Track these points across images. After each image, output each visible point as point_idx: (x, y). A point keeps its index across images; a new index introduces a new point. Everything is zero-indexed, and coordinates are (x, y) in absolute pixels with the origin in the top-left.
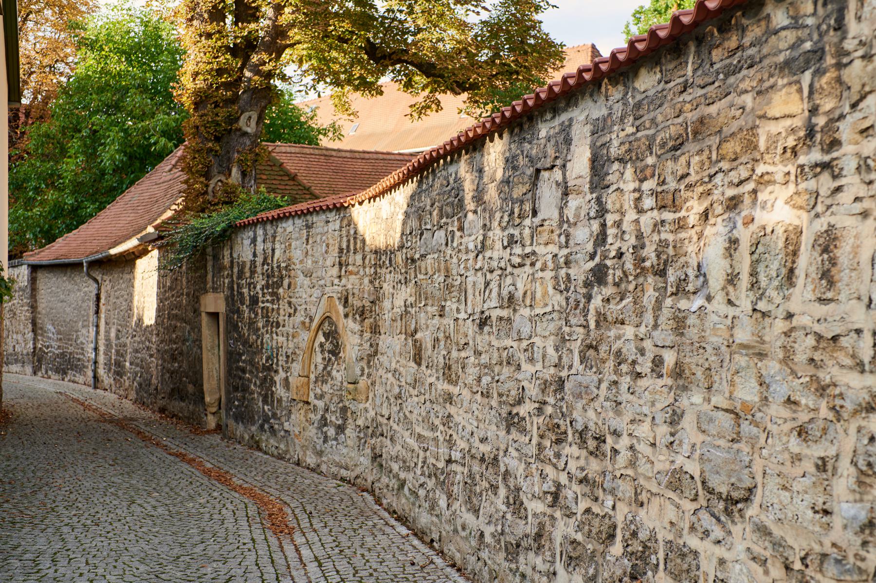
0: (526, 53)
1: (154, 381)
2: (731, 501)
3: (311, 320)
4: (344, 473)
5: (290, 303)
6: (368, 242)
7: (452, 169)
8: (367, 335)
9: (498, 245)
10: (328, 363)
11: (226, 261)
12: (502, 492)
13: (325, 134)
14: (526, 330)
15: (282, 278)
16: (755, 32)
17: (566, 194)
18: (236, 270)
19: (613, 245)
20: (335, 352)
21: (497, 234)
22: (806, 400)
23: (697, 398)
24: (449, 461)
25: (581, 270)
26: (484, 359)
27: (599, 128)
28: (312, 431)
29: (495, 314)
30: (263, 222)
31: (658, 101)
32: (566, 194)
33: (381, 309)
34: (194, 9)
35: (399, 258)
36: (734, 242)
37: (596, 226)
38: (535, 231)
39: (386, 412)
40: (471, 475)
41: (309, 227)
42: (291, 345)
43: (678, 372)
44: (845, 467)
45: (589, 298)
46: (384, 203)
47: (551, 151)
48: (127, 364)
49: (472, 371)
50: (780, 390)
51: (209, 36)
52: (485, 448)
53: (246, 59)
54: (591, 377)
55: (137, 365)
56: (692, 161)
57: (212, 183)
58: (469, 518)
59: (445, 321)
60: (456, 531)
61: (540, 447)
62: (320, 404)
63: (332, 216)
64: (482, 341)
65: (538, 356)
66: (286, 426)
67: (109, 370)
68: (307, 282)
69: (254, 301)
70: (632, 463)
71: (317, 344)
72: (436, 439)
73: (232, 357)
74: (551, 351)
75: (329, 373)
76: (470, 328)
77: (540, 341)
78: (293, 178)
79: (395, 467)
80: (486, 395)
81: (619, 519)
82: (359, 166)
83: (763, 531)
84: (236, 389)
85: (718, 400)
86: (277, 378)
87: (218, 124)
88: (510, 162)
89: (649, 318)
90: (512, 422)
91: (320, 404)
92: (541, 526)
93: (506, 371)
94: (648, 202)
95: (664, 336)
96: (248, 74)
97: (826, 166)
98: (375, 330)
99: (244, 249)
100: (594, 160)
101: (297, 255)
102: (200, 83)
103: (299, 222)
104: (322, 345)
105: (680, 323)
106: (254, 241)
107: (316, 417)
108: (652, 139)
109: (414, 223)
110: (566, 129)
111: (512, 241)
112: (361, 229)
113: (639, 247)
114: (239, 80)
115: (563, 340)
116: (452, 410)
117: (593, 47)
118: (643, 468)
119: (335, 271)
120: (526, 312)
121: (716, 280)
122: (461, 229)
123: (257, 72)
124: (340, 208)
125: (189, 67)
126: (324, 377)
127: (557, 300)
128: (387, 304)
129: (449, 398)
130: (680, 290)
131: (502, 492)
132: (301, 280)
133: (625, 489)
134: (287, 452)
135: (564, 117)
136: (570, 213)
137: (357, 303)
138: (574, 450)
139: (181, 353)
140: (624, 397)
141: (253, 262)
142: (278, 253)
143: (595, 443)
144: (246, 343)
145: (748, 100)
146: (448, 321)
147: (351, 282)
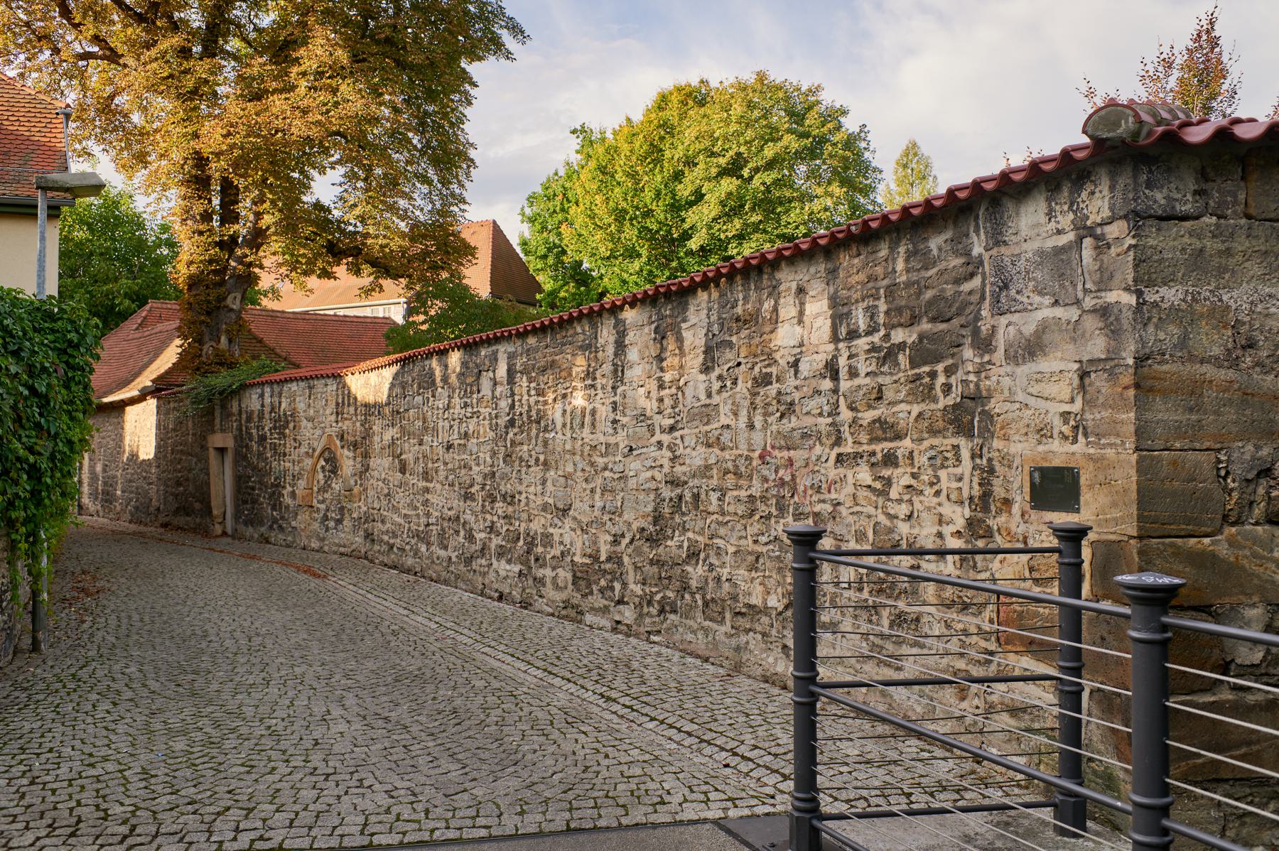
0: (448, 253)
1: (155, 503)
2: (565, 510)
3: (314, 450)
4: (342, 550)
5: (295, 440)
6: (359, 398)
7: (427, 362)
8: (359, 459)
9: (458, 407)
10: (328, 479)
11: (235, 409)
12: (462, 533)
13: (265, 296)
14: (475, 450)
15: (287, 422)
16: (571, 332)
17: (495, 384)
18: (244, 416)
19: (518, 410)
20: (334, 471)
21: (456, 401)
22: (588, 469)
23: (552, 473)
24: (428, 525)
25: (503, 421)
26: (450, 466)
27: (511, 357)
28: (316, 525)
29: (456, 442)
30: (271, 383)
31: (537, 350)
32: (495, 384)
33: (371, 442)
34: (187, 212)
35: (387, 410)
36: (565, 411)
37: (510, 401)
38: (479, 400)
39: (376, 505)
40: (443, 529)
41: (310, 388)
42: (297, 468)
43: (545, 463)
44: (598, 490)
45: (507, 433)
46: (373, 376)
47: (487, 362)
48: (119, 493)
49: (442, 474)
50: (580, 466)
51: (201, 233)
52: (450, 513)
53: (231, 252)
54: (508, 469)
55: (131, 492)
56: (549, 377)
57: (205, 348)
58: (442, 553)
59: (423, 448)
60: (433, 562)
61: (483, 506)
62: (323, 506)
63: (329, 381)
64: (448, 457)
65: (481, 462)
66: (293, 524)
67: (96, 499)
68: (310, 425)
69: (263, 438)
70: (527, 504)
71: (319, 467)
72: (418, 515)
73: (240, 480)
74: (488, 459)
75: (329, 486)
76: (441, 451)
77: (481, 454)
78: (260, 341)
79: (386, 538)
80: (452, 485)
81: (522, 530)
82: (301, 325)
83: (575, 519)
84: (245, 502)
85: (560, 473)
86: (285, 492)
87: (209, 302)
88: (464, 364)
89: (533, 441)
90: (468, 497)
91: (323, 506)
92: (484, 544)
93: (463, 472)
94: (533, 392)
95: (539, 449)
96: (233, 264)
97: (593, 386)
98: (366, 455)
99: (253, 401)
100: (509, 370)
101: (301, 406)
102: (193, 269)
103: (302, 384)
104: (323, 467)
105: (546, 443)
106: (262, 396)
107: (319, 516)
108: (534, 365)
109: (398, 390)
110: (495, 353)
111: (466, 405)
112: (353, 390)
113: (529, 411)
114: (225, 268)
115: (494, 454)
116: (429, 496)
117: (494, 222)
118: (532, 505)
119: (333, 418)
120: (475, 441)
121: (559, 426)
122: (433, 396)
123: (241, 263)
124: (337, 377)
125: (184, 257)
126: (326, 488)
127: (491, 434)
128: (376, 439)
129: (427, 490)
130: (546, 430)
131: (462, 533)
132: (304, 423)
133: (524, 516)
134: (294, 542)
135: (494, 348)
136: (497, 393)
137: (351, 439)
138: (501, 504)
139: (187, 480)
140: (524, 476)
141: (261, 413)
142: (283, 405)
143: (510, 499)
144: (254, 468)
145: (569, 356)
146: (425, 447)
147: (346, 425)
